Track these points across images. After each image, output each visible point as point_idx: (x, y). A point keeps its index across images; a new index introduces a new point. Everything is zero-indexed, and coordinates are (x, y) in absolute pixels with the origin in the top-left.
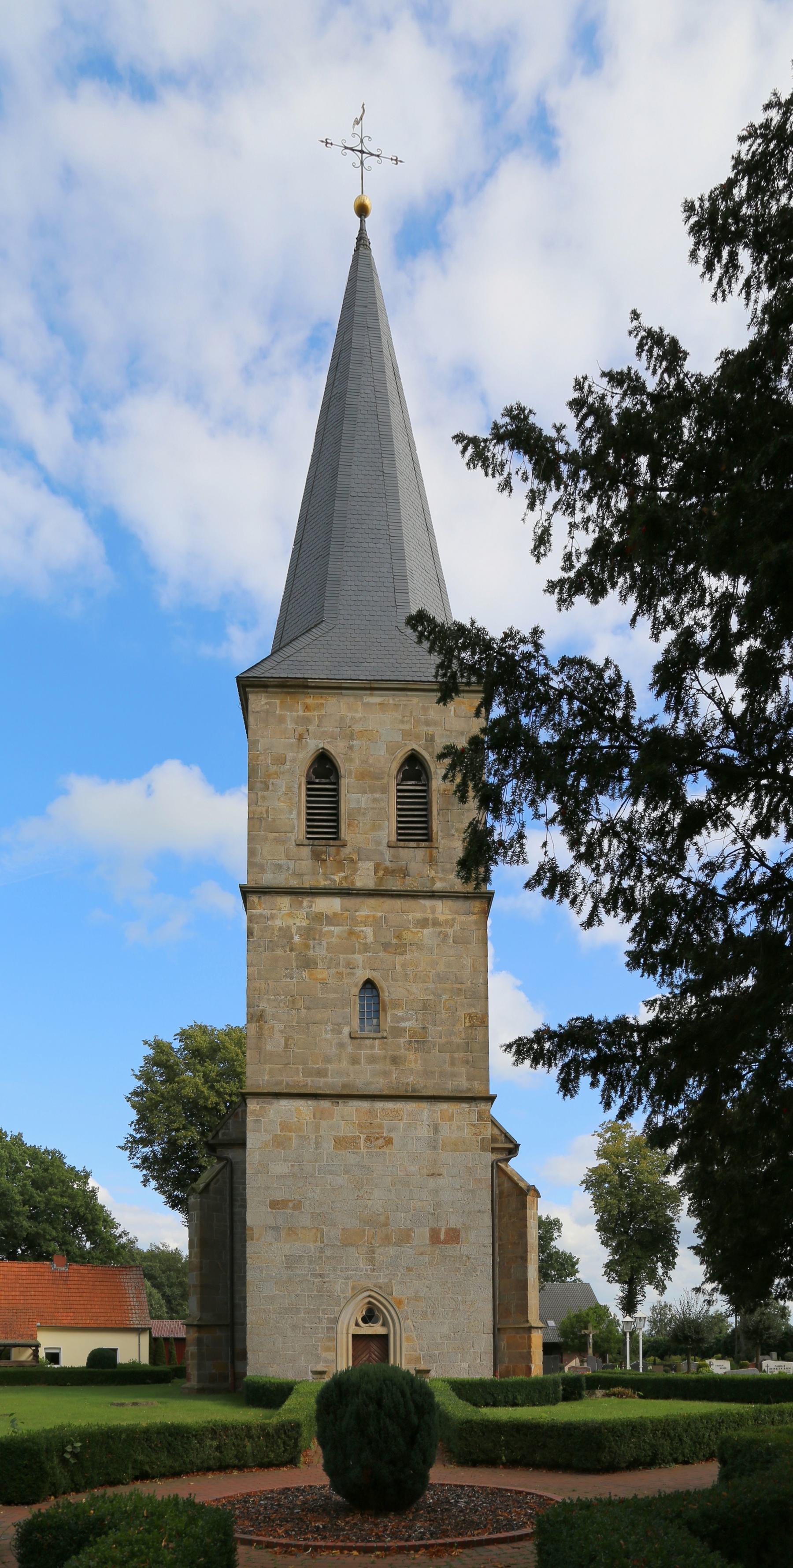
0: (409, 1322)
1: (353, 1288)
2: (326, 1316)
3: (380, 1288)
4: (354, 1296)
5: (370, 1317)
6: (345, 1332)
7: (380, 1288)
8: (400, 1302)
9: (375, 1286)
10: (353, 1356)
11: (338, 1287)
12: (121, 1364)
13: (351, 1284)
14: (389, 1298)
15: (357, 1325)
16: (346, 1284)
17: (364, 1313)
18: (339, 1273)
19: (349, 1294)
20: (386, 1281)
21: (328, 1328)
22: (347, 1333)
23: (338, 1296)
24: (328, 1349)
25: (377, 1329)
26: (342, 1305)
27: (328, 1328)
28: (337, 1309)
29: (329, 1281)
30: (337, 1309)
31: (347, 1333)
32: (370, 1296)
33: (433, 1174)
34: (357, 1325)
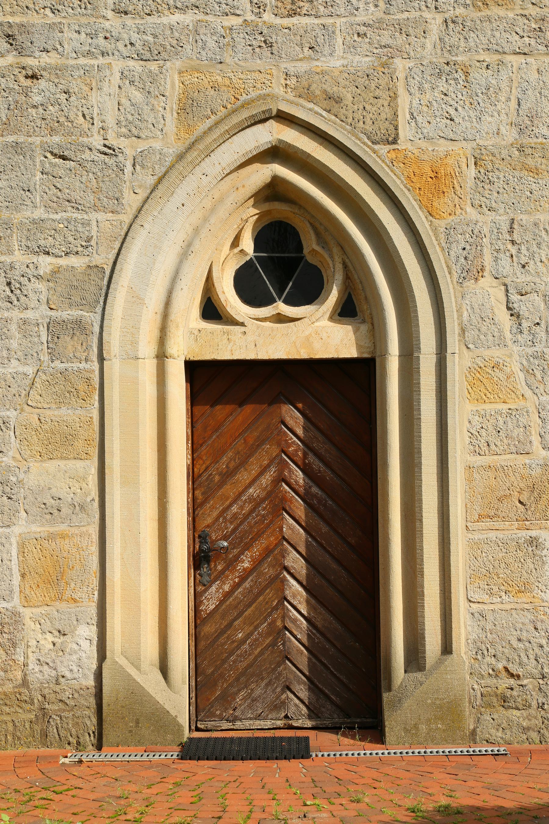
0: (488, 293)
1: (187, 107)
2: (46, 264)
3: (332, 101)
4: (191, 152)
5: (285, 260)
6: (147, 348)
7: (332, 101)
8: (437, 181)
9: (306, 94)
10: (194, 478)
11: (105, 102)
12: (359, 347)
13: (172, 84)
14: (377, 158)
15: (211, 311)
16: (150, 86)
17: (248, 244)
18: (113, 23)
19: (166, 140)
20: (363, 61)
21: (55, 329)
22: (162, 356)
23: (109, 151)
24: (57, 443)
25: (316, 333)
26: (132, 201)
27: (55, 329)
28: (103, 224)
29: (59, 71)
30: (103, 224)
31: (162, 356)
32: (276, 153)
33: (97, 222)
34: (211, 311)
